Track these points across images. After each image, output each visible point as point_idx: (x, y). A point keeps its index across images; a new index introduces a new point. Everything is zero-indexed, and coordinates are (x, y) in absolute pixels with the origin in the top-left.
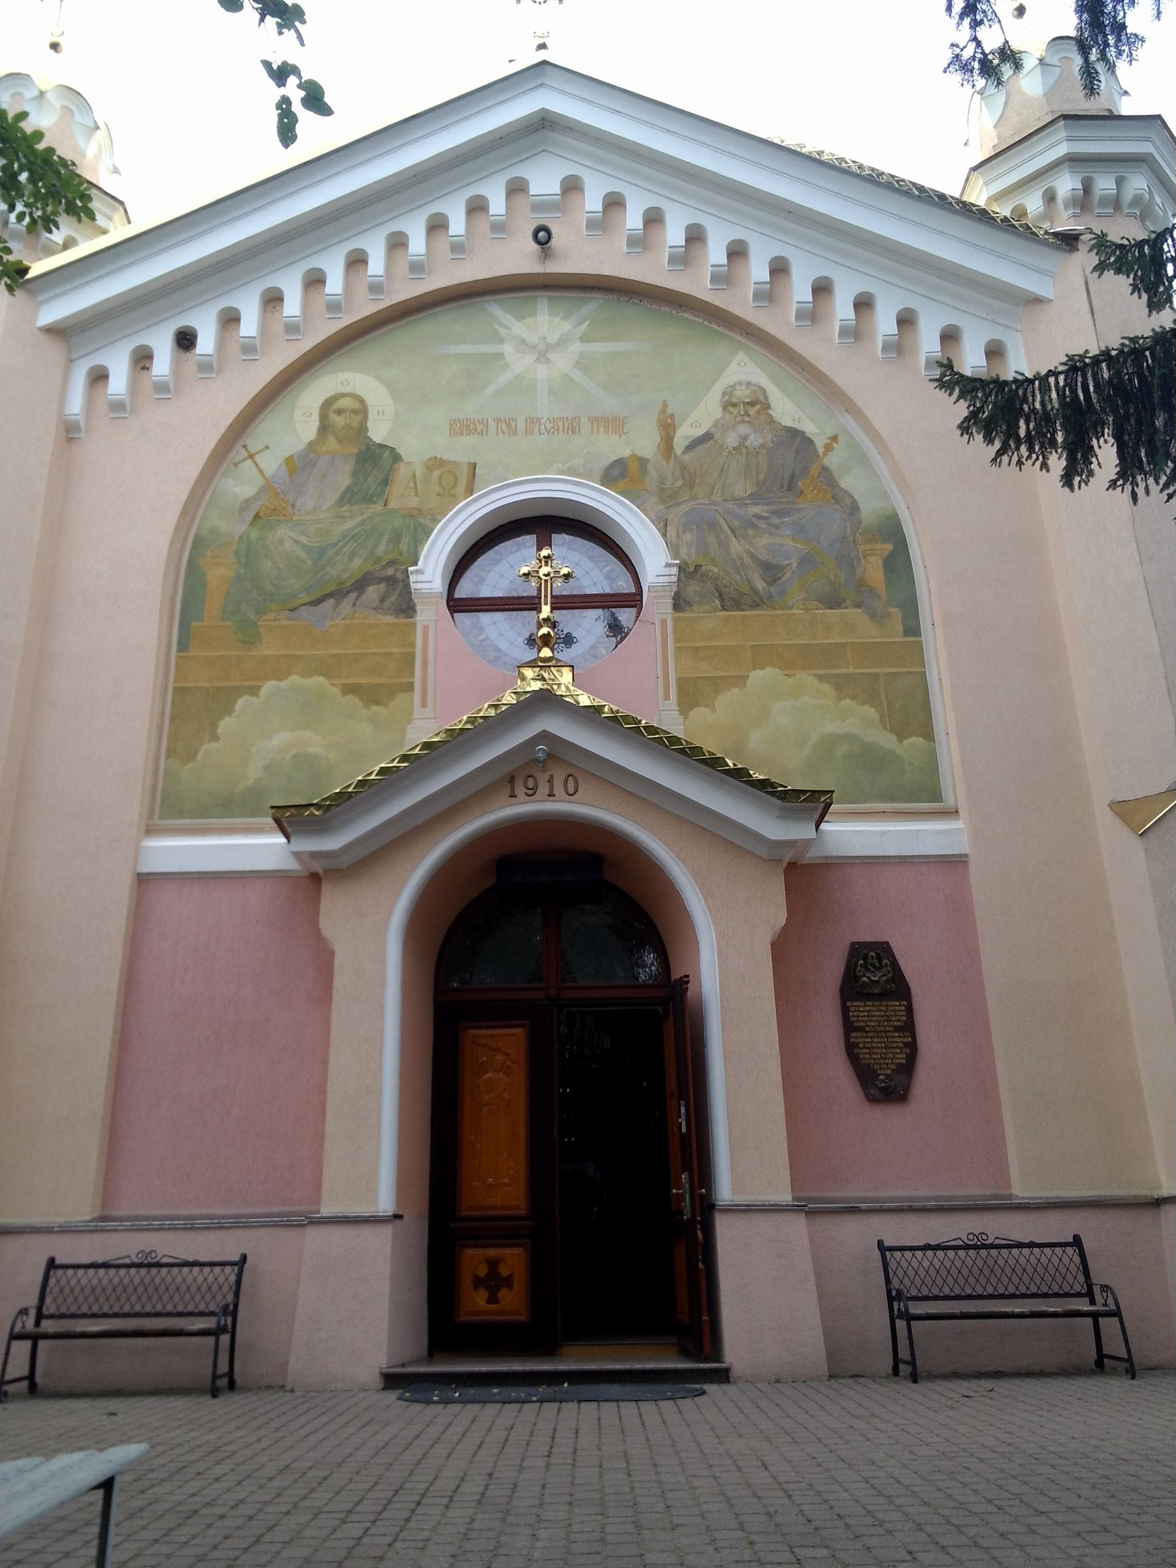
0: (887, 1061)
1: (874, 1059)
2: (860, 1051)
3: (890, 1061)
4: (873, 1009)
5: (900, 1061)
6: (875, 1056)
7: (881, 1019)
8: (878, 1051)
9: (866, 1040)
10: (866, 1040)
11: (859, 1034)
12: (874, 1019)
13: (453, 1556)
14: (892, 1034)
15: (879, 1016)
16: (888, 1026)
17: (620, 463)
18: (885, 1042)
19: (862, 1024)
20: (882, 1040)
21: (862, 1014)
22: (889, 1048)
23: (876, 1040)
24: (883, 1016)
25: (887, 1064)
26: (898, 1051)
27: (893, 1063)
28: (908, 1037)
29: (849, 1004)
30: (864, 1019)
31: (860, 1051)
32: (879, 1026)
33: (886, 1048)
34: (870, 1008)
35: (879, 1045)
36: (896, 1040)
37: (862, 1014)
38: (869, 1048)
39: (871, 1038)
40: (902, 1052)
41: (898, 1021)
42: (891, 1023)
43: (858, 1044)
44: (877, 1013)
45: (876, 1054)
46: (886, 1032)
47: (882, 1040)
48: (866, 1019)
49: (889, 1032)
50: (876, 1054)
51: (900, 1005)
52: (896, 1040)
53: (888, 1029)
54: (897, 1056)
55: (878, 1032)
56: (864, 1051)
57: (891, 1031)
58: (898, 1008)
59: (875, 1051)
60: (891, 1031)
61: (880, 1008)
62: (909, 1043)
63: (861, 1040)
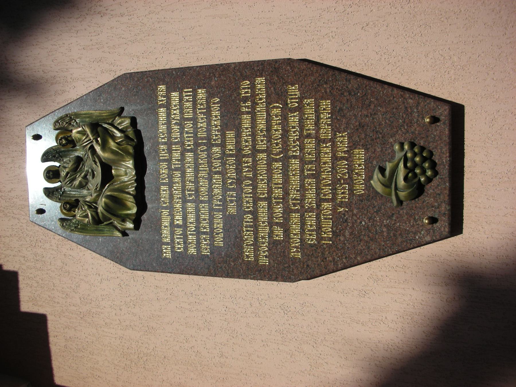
0: (327, 158)
1: (320, 201)
2: (296, 240)
3: (327, 149)
4: (177, 186)
5: (325, 116)
6: (311, 196)
7: (204, 167)
8: (295, 181)
9: (263, 216)
10: (263, 216)
11: (248, 237)
12: (204, 184)
13: (100, 6)
14: (246, 134)
15: (197, 170)
16: (223, 145)
17: (41, 214)
18: (270, 162)
19: (219, 224)
20: (262, 168)
21: (191, 218)
22: (285, 149)
23: (262, 186)
24: (196, 158)
25: (335, 158)
26: (294, 119)
27: (333, 141)
28: (253, 87)
29: (260, 81)
30: (205, 216)
31: (296, 240)
32: (223, 173)
33: (286, 160)
34: (177, 194)
35: (278, 178)
36: (261, 124)
37: (191, 218)
38: (287, 212)
39: (256, 200)
40: (300, 109)
41: (208, 113)
42: (215, 132)
43: (273, 244)
44: (190, 172)
45: (303, 189)
46: (239, 154)
47: (262, 168)
48: (204, 209)
49: (238, 143)
50: (303, 189)
51: (168, 106)
52: (261, 124)
53: (230, 147)
54: (310, 126)
55: (239, 181)
56: (295, 228)
57: (238, 136)
58: (176, 112)
59: (294, 194)
60: (238, 136)
61: (176, 164)
62: (269, 83)
63: (264, 231)
